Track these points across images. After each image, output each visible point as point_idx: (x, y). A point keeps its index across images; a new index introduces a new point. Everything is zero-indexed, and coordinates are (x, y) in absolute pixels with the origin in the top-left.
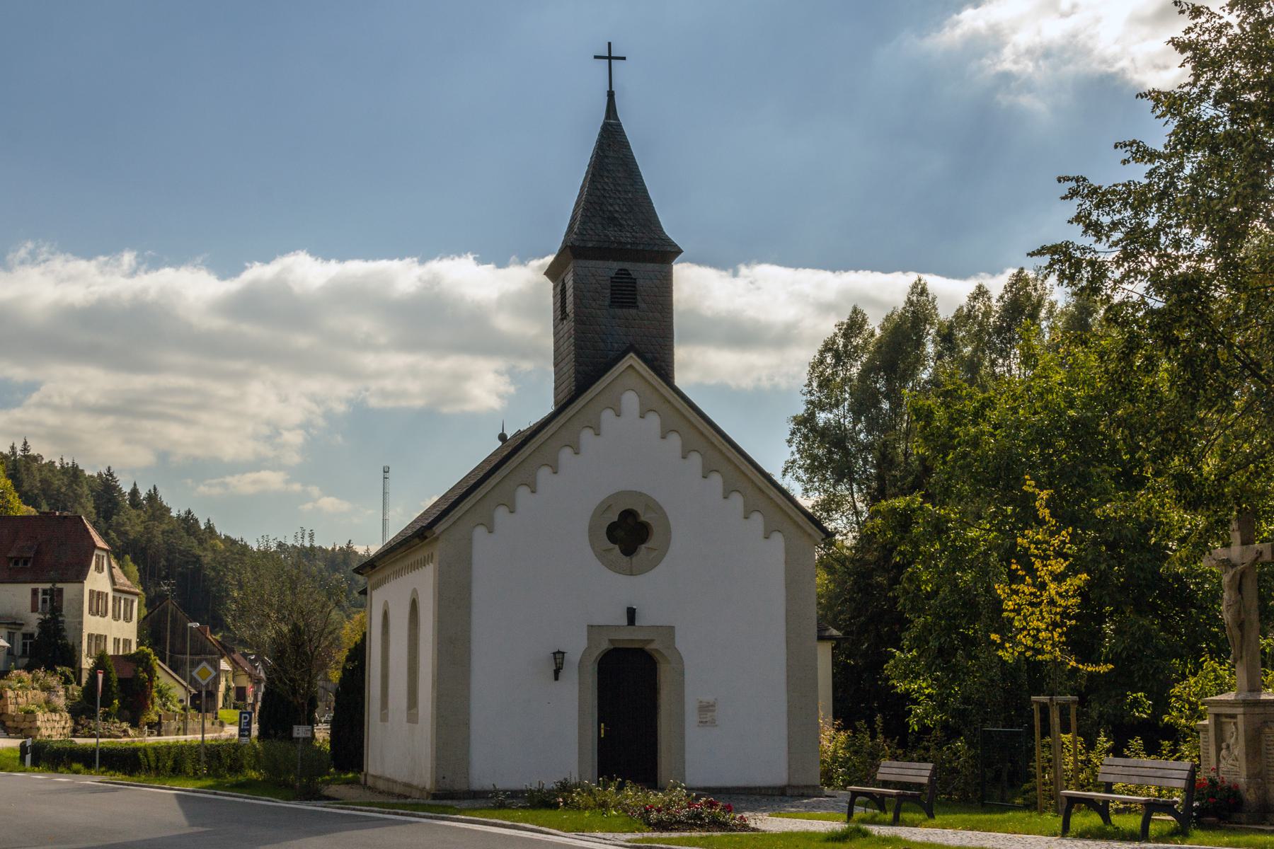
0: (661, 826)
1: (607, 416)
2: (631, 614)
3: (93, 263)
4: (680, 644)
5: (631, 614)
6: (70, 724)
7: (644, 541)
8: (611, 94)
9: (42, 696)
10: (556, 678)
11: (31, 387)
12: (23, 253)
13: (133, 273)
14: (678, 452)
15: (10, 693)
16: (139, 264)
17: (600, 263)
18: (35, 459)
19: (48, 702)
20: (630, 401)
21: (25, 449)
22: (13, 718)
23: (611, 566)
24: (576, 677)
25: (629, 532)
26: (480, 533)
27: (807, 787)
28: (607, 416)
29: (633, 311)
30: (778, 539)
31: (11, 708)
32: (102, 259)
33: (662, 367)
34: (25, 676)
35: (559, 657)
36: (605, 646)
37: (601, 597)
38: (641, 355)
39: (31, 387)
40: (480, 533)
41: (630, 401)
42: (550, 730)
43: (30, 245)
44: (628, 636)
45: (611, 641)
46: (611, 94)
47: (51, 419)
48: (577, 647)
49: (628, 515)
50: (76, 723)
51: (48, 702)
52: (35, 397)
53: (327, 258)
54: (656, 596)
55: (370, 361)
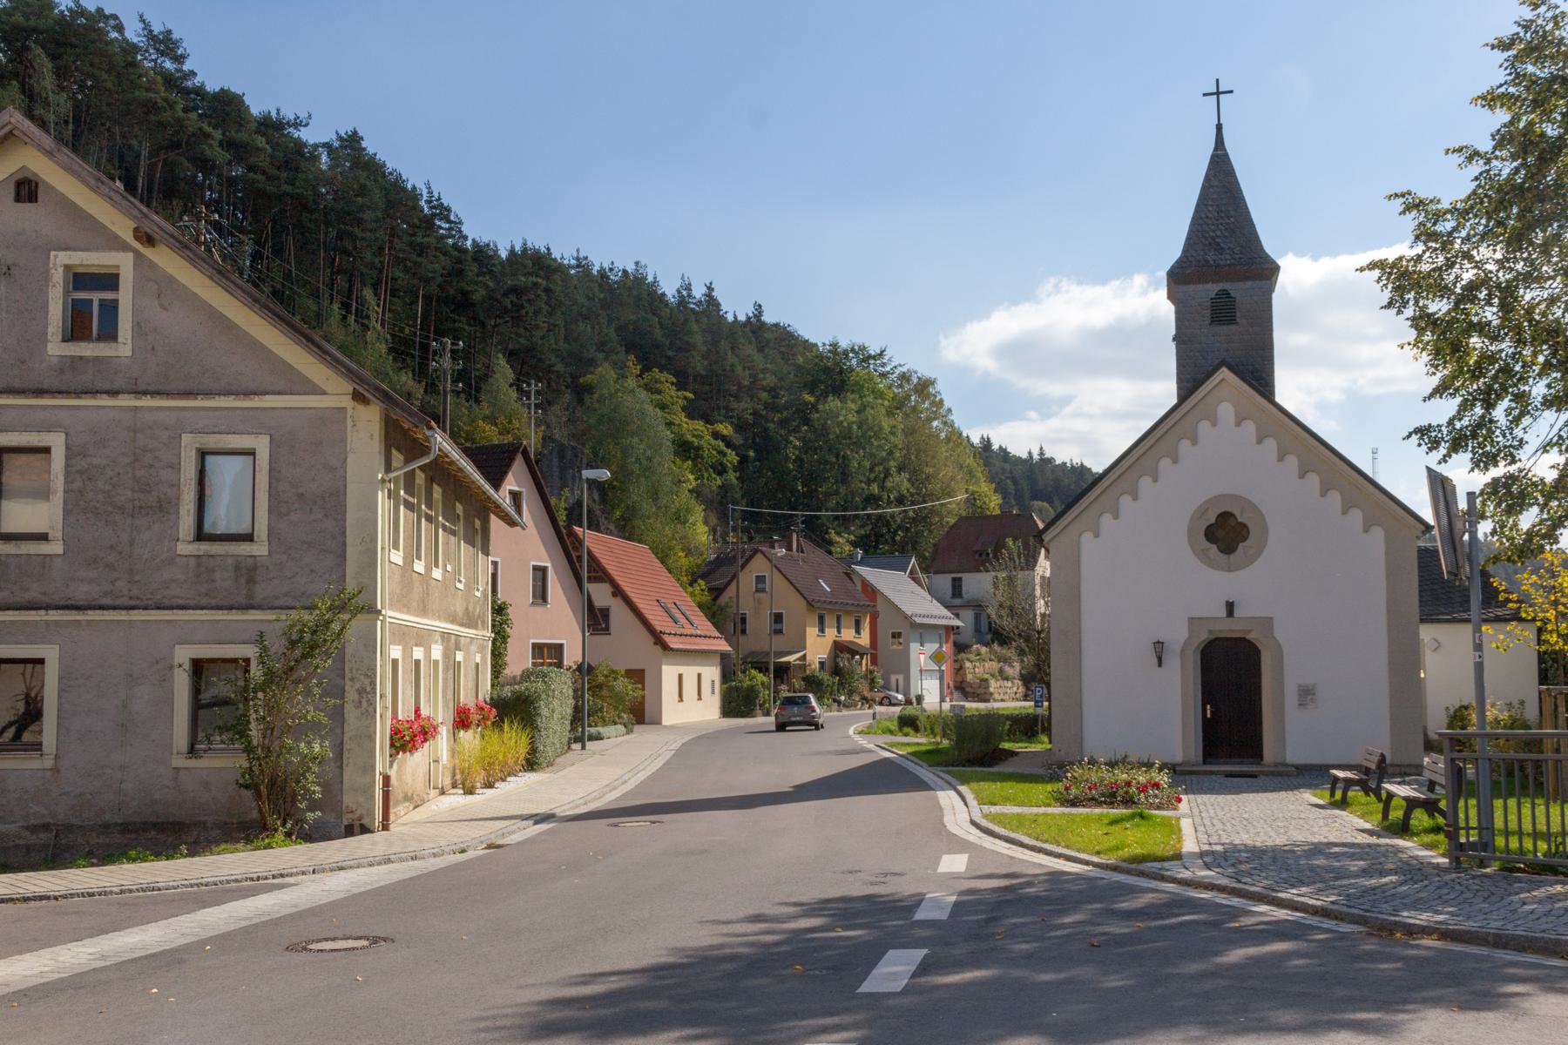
0: (1074, 803)
1: (1204, 426)
2: (1230, 607)
3: (1107, 288)
4: (1279, 633)
5: (1230, 607)
6: (1022, 690)
7: (1245, 539)
8: (1219, 127)
9: (995, 665)
10: (1160, 665)
11: (1065, 401)
12: (1049, 287)
13: (1145, 292)
14: (1275, 456)
15: (968, 664)
16: (1150, 284)
17: (1200, 287)
18: (1051, 460)
19: (1001, 671)
20: (1226, 411)
21: (1042, 454)
22: (971, 685)
23: (1210, 563)
24: (1178, 660)
25: (1226, 533)
26: (1087, 537)
27: (1409, 766)
28: (1204, 426)
29: (1232, 327)
30: (1378, 534)
31: (969, 677)
32: (1115, 283)
33: (1259, 376)
34: (984, 650)
35: (1159, 646)
36: (1204, 636)
37: (1201, 593)
38: (1231, 368)
39: (1065, 401)
40: (1087, 537)
41: (1226, 411)
42: (1168, 712)
43: (1053, 280)
44: (1228, 628)
45: (1210, 632)
46: (1219, 127)
47: (1080, 425)
48: (1177, 635)
49: (1225, 517)
50: (1028, 689)
51: (1001, 671)
52: (1068, 410)
53: (1316, 258)
54: (1257, 591)
55: (1366, 351)
